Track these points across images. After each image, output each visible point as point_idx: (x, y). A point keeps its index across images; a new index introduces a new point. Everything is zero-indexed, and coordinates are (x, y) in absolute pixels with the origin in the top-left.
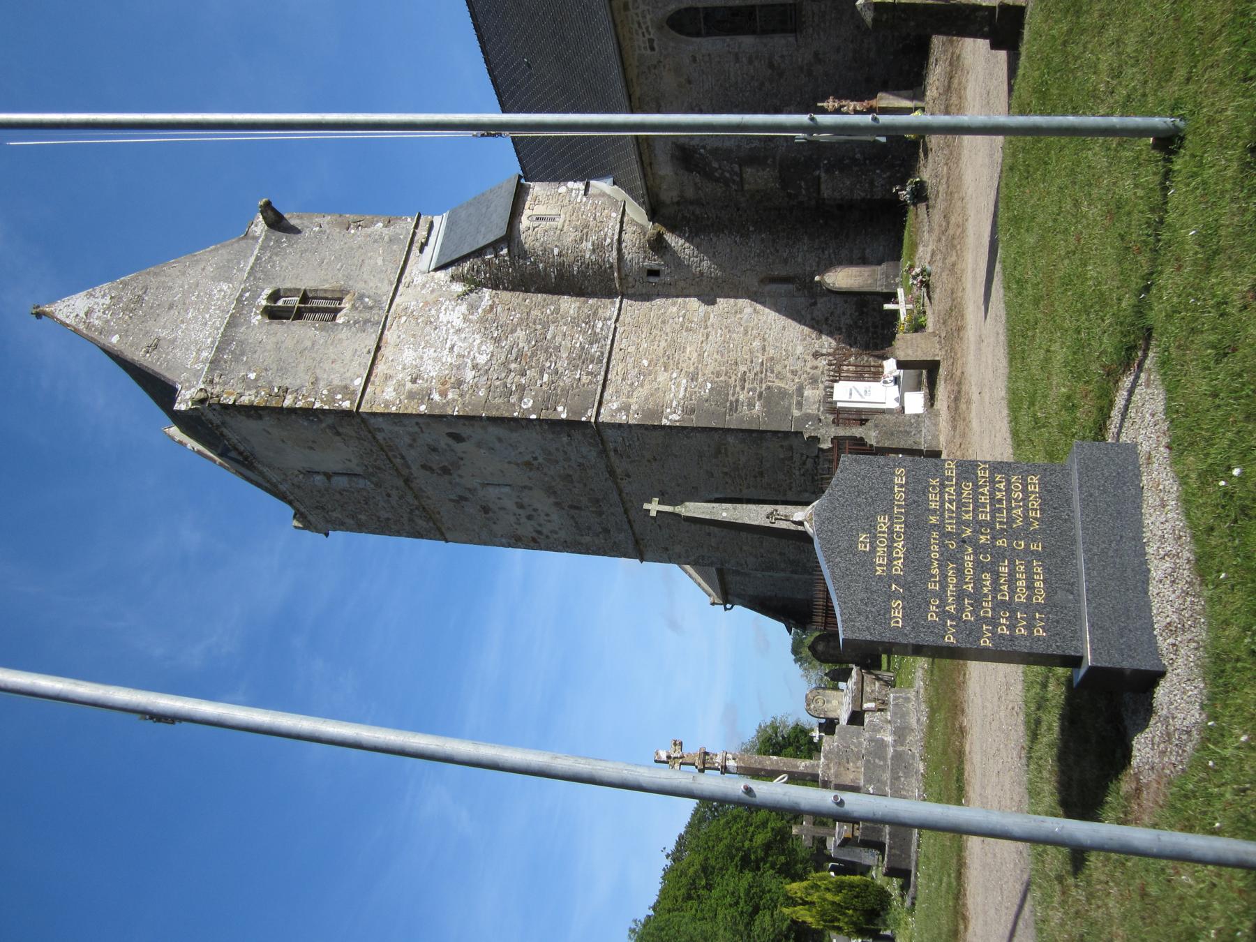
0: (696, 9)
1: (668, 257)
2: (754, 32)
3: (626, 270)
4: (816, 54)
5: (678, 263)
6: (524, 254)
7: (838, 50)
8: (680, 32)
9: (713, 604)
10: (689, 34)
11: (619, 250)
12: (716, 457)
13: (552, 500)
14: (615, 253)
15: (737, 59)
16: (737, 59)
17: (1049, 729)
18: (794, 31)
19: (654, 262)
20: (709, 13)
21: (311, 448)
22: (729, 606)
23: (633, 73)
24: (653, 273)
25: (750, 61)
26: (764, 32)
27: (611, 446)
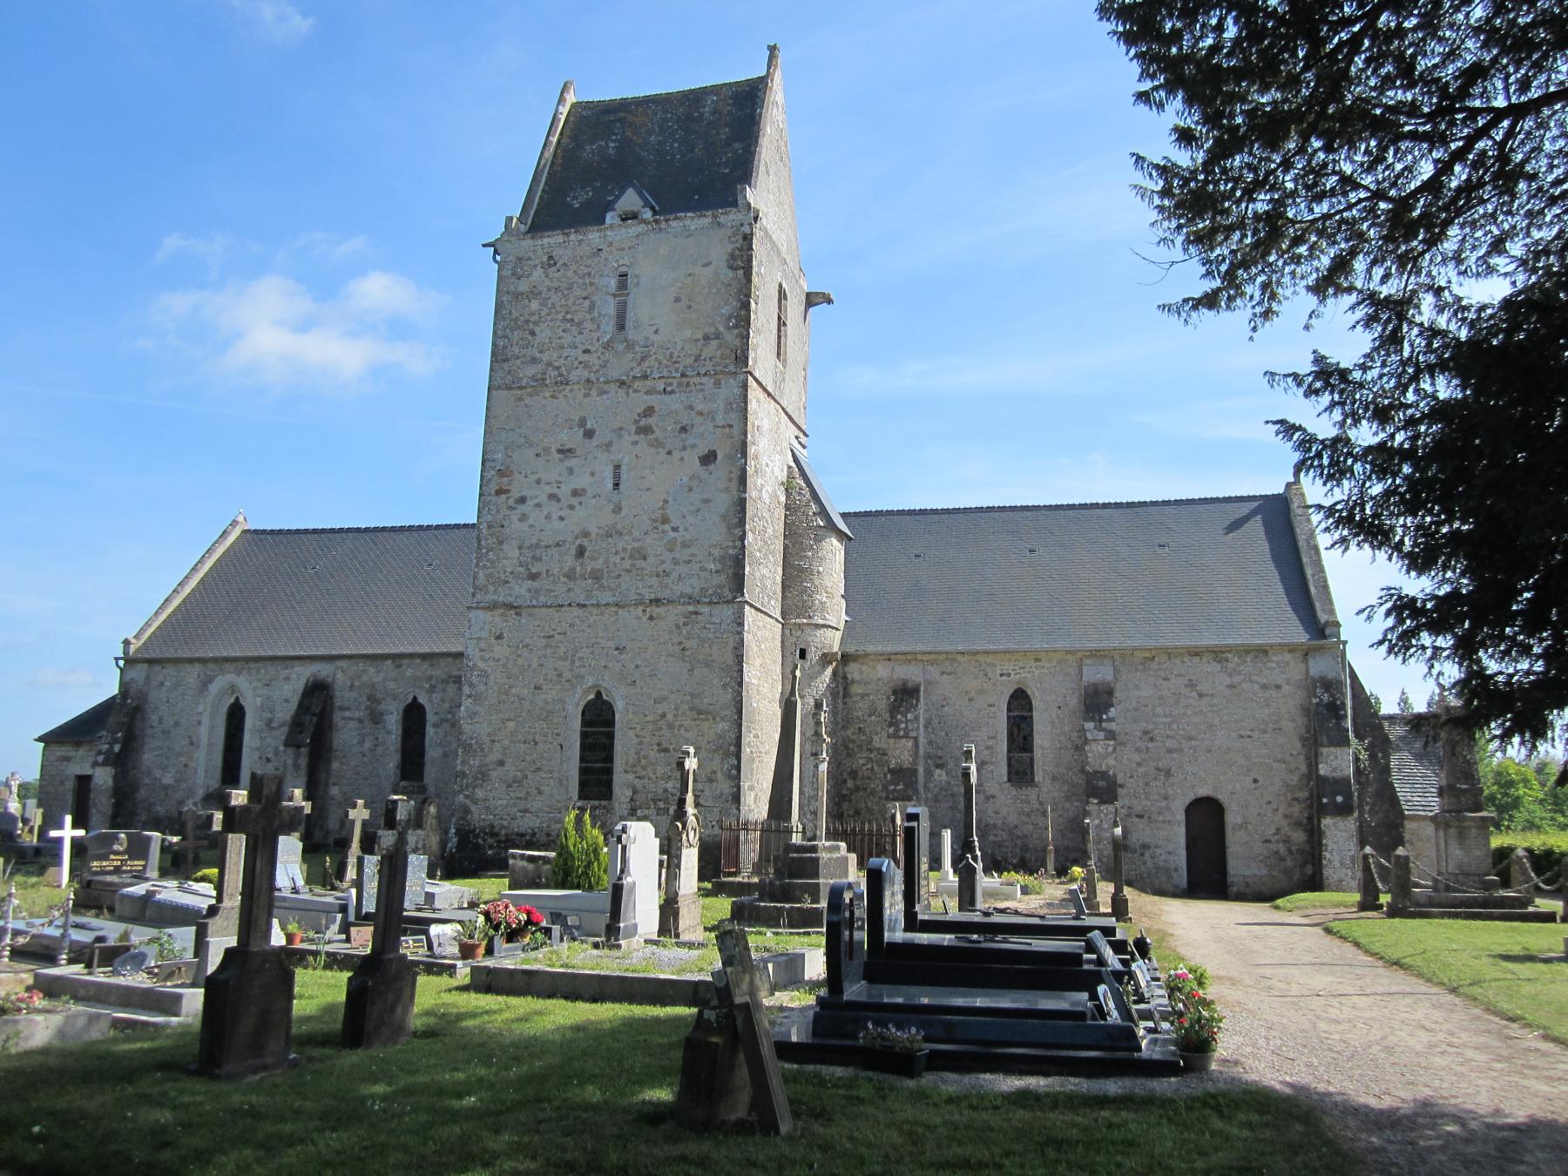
0: (1031, 710)
1: (818, 668)
2: (1009, 751)
3: (808, 630)
4: (993, 797)
5: (811, 677)
6: (818, 540)
7: (997, 813)
8: (1012, 697)
9: (127, 643)
10: (1009, 703)
11: (824, 626)
12: (691, 709)
13: (594, 531)
14: (821, 622)
15: (990, 738)
16: (990, 738)
17: (792, 999)
18: (1009, 780)
19: (814, 656)
20: (1028, 720)
21: (678, 300)
22: (121, 663)
23: (981, 658)
24: (803, 654)
25: (988, 748)
26: (1009, 759)
27: (705, 609)
